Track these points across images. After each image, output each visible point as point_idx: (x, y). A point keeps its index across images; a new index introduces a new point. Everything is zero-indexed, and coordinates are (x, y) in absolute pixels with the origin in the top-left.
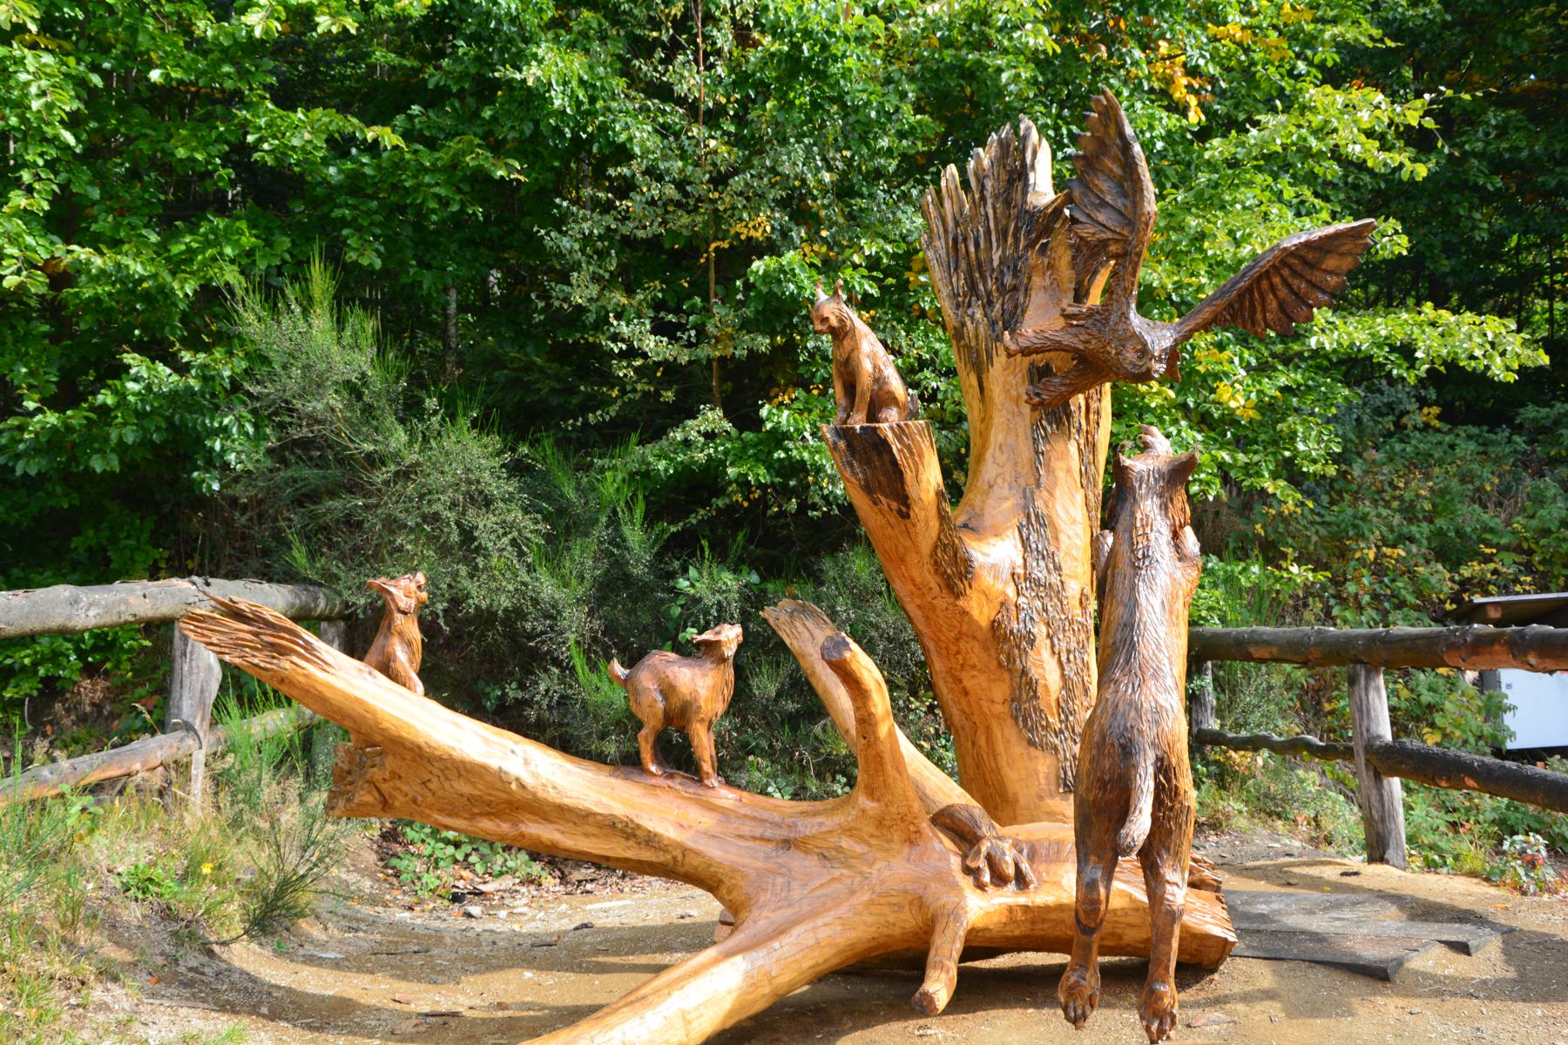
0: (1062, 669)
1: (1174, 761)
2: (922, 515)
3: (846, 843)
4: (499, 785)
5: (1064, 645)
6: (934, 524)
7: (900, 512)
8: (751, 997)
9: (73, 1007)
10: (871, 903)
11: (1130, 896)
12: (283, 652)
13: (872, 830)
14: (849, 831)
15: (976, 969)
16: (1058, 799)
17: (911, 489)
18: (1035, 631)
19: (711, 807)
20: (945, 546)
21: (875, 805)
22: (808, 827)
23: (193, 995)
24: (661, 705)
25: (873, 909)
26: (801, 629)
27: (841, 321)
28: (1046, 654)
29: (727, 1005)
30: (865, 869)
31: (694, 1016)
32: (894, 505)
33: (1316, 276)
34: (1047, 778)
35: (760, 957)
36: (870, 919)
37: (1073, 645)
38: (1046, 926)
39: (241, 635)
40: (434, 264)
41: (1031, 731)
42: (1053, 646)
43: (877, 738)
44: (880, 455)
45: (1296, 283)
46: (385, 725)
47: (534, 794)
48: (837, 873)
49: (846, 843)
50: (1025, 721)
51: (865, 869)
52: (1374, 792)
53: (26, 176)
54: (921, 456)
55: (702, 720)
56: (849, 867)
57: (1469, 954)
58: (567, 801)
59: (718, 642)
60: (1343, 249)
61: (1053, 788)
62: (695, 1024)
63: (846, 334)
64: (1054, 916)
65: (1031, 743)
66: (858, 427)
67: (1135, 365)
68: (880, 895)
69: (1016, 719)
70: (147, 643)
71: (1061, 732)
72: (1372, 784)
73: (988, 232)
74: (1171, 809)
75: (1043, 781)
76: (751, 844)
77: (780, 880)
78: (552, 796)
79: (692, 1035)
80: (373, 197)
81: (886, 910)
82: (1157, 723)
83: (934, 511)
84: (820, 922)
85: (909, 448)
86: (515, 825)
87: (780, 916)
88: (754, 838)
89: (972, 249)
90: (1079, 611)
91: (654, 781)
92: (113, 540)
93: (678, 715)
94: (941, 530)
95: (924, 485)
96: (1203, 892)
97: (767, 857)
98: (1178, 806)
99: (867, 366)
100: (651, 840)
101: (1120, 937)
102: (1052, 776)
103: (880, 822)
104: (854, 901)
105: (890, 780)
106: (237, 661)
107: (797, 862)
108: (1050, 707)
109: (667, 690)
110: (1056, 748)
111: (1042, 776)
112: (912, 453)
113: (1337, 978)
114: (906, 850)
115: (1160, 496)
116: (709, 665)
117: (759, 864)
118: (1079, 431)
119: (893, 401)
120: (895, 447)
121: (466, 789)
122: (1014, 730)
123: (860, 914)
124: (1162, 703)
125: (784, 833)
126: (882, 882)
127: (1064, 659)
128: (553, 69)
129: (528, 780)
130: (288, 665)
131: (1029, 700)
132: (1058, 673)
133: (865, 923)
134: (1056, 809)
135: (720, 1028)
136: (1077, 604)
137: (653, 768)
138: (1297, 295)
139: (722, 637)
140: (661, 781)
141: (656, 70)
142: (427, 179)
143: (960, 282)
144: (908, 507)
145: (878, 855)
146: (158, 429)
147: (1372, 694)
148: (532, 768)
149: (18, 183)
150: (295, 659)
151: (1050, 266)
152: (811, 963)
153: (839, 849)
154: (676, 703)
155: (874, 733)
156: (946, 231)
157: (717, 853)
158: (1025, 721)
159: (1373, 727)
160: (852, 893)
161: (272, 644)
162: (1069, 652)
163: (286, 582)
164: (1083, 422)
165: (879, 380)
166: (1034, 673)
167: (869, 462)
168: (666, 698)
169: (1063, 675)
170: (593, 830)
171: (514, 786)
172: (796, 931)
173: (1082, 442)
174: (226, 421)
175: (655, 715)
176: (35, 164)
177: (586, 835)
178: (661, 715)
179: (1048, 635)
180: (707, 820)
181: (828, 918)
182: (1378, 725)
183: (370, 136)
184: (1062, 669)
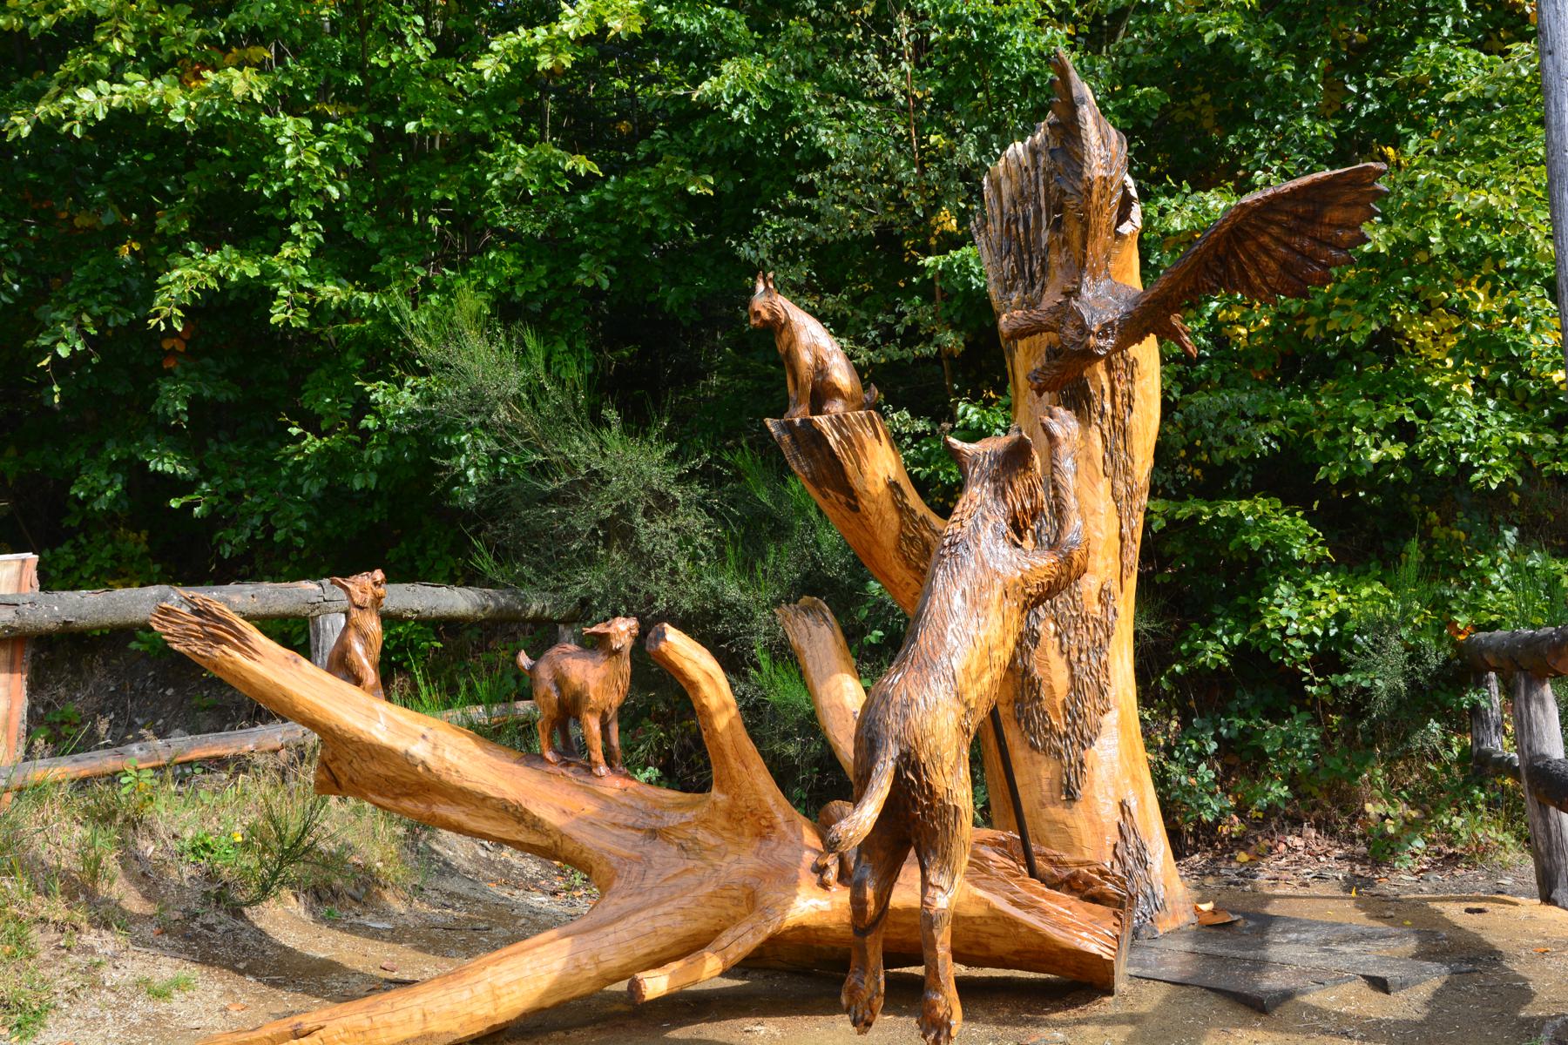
0: (1072, 669)
1: (923, 757)
2: (872, 508)
3: (701, 835)
4: (407, 767)
5: (1074, 644)
6: (892, 518)
7: (848, 505)
8: (573, 979)
9: (59, 947)
10: (714, 895)
11: (988, 903)
12: (219, 640)
13: (724, 823)
14: (704, 823)
15: (912, 975)
16: (1060, 808)
17: (856, 483)
18: (1040, 628)
19: (598, 796)
20: (912, 540)
21: (723, 797)
22: (672, 819)
23: (186, 948)
24: (555, 696)
25: (715, 901)
26: (801, 626)
27: (773, 314)
28: (1052, 653)
29: (544, 984)
30: (716, 862)
31: (504, 991)
32: (842, 498)
33: (1321, 232)
34: (1050, 784)
35: (591, 942)
36: (712, 911)
37: (1086, 643)
38: (899, 930)
39: (191, 626)
40: (685, 280)
41: (1033, 734)
42: (1061, 644)
43: (715, 730)
44: (819, 447)
45: (1296, 241)
46: (301, 708)
47: (438, 777)
48: (691, 864)
49: (701, 835)
50: (1027, 724)
51: (716, 862)
52: (1539, 820)
53: (295, 228)
54: (862, 447)
55: (592, 711)
56: (702, 859)
57: (1388, 992)
58: (466, 784)
59: (607, 635)
60: (1344, 199)
61: (1055, 795)
62: (504, 1000)
63: (783, 326)
64: (906, 920)
65: (1033, 747)
66: (797, 420)
67: (1075, 343)
68: (723, 888)
69: (1019, 721)
70: (439, 645)
71: (1067, 735)
72: (1536, 811)
73: (1038, 211)
74: (931, 807)
75: (1045, 787)
76: (622, 832)
77: (636, 868)
78: (454, 779)
79: (501, 1010)
80: (613, 221)
81: (727, 903)
82: (906, 717)
83: (888, 503)
84: (660, 911)
85: (848, 440)
86: (429, 806)
87: (628, 903)
88: (627, 827)
89: (1021, 230)
90: (1098, 608)
91: (549, 769)
92: (422, 551)
93: (570, 708)
94: (902, 523)
95: (869, 477)
96: (1098, 907)
97: (635, 846)
98: (937, 805)
99: (806, 358)
100: (536, 825)
101: (987, 948)
102: (1056, 782)
103: (729, 815)
104: (699, 892)
105: (734, 773)
106: (182, 649)
107: (660, 853)
108: (1055, 710)
109: (560, 681)
110: (1059, 753)
111: (1044, 782)
112: (851, 445)
113: (1221, 1004)
114: (757, 844)
115: (994, 480)
116: (601, 657)
117: (625, 852)
118: (1102, 414)
119: (836, 392)
120: (833, 439)
121: (381, 770)
122: (1018, 733)
123: (703, 905)
124: (914, 696)
125: (652, 822)
126: (729, 874)
127: (1074, 657)
128: (732, 82)
129: (433, 763)
130: (217, 653)
131: (1032, 701)
132: (1067, 673)
133: (706, 915)
134: (1057, 817)
135: (538, 1006)
136: (1096, 600)
137: (549, 755)
138: (1302, 254)
139: (611, 630)
140: (557, 769)
141: (854, 73)
142: (643, 200)
143: (1009, 264)
144: (855, 499)
145: (730, 848)
146: (409, 448)
147: (1534, 706)
148: (439, 752)
149: (288, 236)
150: (224, 647)
151: (1065, 242)
152: (647, 950)
153: (695, 840)
154: (568, 693)
155: (711, 725)
156: (1002, 213)
157: (591, 841)
158: (1027, 724)
159: (1536, 745)
160: (701, 884)
161: (212, 635)
162: (1080, 651)
163: (467, 584)
164: (1108, 406)
165: (821, 370)
166: (1037, 672)
167: (811, 456)
168: (560, 689)
169: (1072, 677)
170: (491, 813)
171: (420, 769)
172: (633, 919)
173: (1106, 427)
174: (463, 438)
175: (549, 704)
176: (305, 217)
177: (487, 818)
178: (554, 705)
179: (1056, 634)
180: (591, 808)
181: (667, 908)
182: (1541, 742)
183: (569, 165)
184: (1072, 669)
